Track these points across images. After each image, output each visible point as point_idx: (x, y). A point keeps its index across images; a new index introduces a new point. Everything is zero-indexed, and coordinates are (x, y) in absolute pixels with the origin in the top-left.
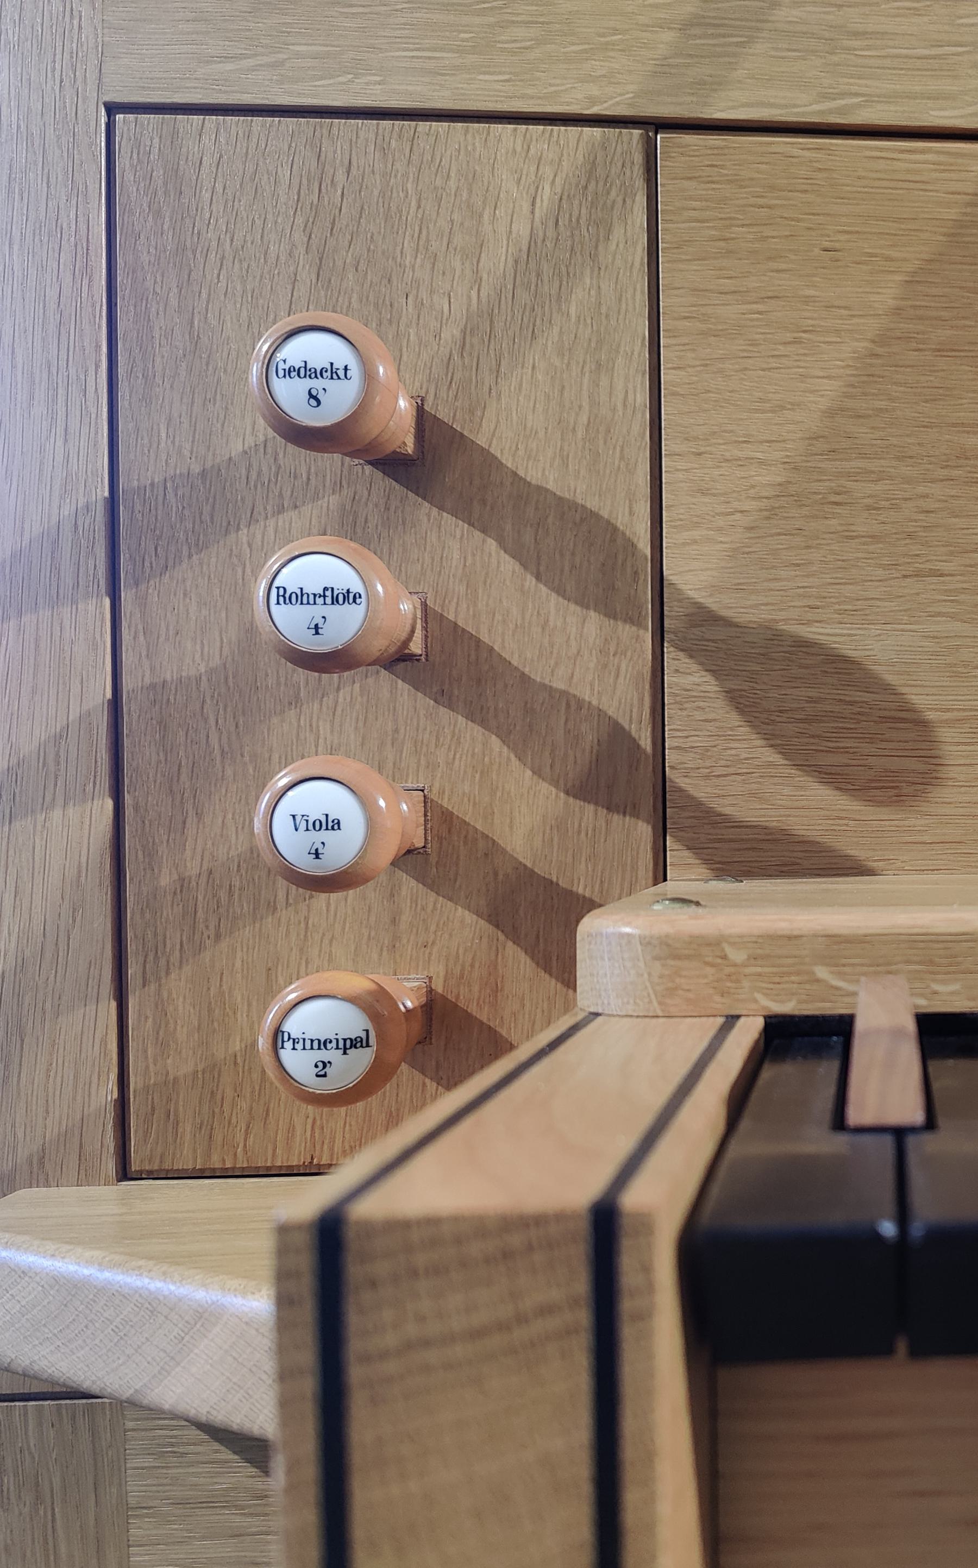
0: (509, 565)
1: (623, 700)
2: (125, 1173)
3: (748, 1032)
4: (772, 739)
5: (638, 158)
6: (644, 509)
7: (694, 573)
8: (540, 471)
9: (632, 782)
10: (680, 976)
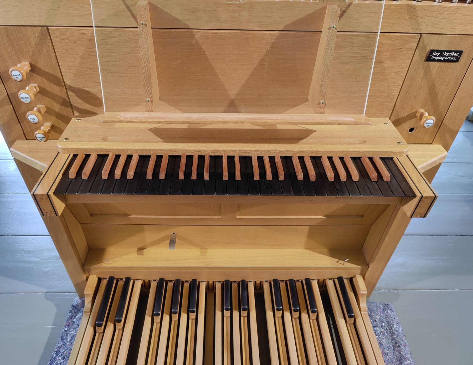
0: (46, 81)
1: (64, 95)
2: (27, 139)
3: (72, 155)
4: (82, 100)
5: (47, 31)
6: (60, 74)
7: (68, 81)
8: (47, 70)
9: (67, 103)
10: (456, 56)
